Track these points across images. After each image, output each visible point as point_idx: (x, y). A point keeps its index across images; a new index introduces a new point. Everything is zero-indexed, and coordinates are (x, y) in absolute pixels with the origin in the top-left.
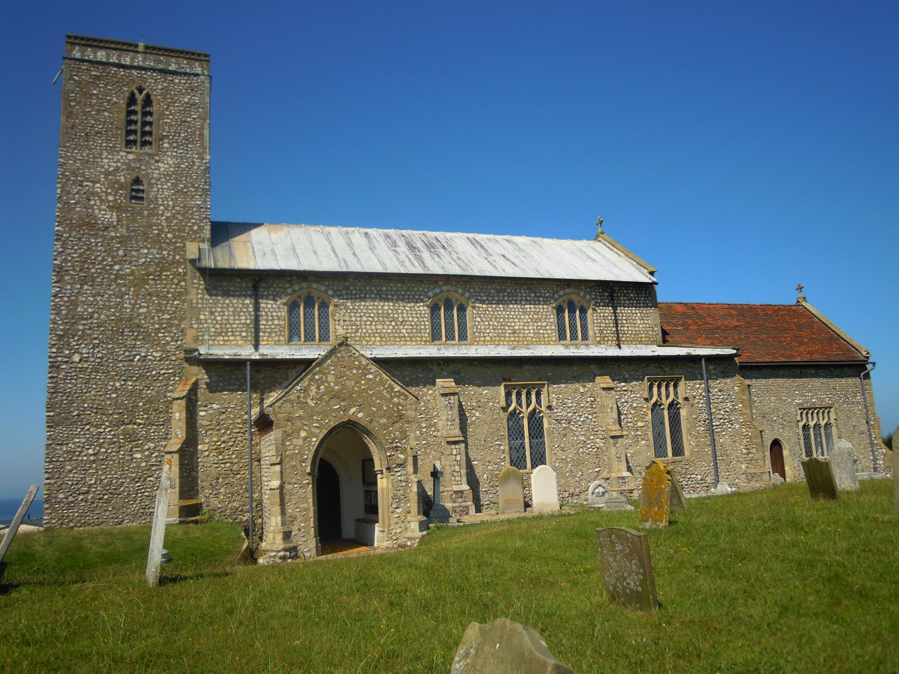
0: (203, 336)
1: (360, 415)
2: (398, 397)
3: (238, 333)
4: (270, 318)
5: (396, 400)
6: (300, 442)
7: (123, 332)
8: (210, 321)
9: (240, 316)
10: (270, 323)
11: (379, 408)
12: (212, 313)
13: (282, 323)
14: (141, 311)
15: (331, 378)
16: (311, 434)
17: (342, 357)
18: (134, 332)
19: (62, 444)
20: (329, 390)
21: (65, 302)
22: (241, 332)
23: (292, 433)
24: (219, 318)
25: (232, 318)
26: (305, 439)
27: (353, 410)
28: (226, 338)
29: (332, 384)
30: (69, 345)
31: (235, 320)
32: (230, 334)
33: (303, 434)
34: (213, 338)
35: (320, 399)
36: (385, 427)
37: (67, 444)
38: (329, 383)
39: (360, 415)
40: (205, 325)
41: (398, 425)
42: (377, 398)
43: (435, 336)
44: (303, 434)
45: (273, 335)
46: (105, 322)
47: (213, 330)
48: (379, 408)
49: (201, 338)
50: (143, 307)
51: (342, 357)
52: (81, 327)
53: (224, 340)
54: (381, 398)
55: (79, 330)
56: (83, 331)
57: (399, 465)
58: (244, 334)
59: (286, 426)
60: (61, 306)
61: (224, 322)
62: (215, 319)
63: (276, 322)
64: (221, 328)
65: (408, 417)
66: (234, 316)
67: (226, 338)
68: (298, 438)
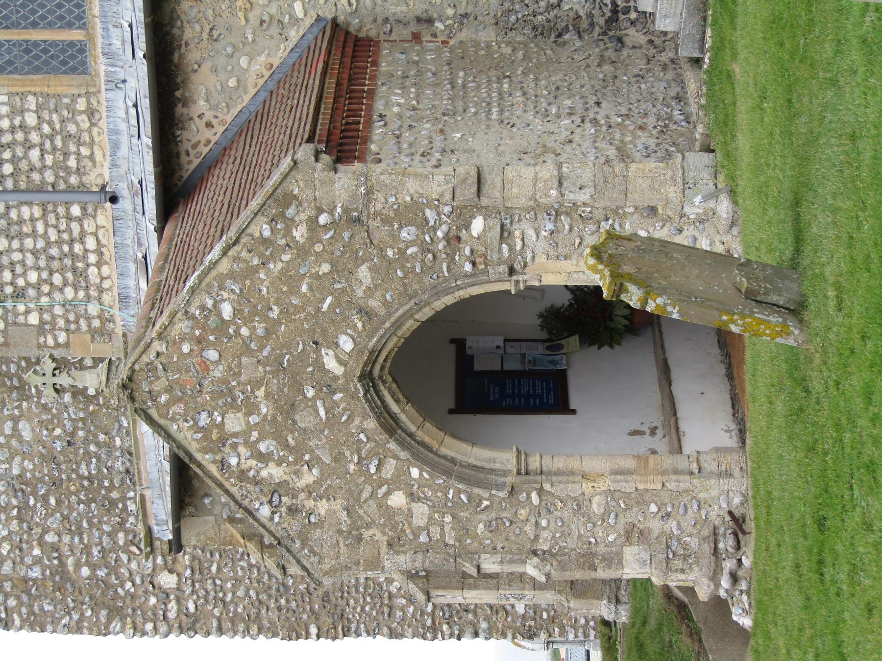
0: (88, 319)
1: (346, 343)
2: (291, 223)
3: (75, 226)
4: (20, 136)
5: (299, 233)
6: (421, 511)
7: (90, 478)
8: (44, 300)
9: (21, 222)
10: (35, 137)
11: (319, 283)
12: (19, 294)
13: (31, 102)
14: (27, 435)
15: (234, 422)
16: (400, 481)
17: (169, 390)
18: (87, 453)
19: (391, 608)
20: (276, 428)
21: (21, 604)
22: (69, 218)
23: (394, 528)
24: (33, 277)
25: (29, 243)
26: (412, 497)
27: (331, 363)
28: (92, 258)
29: (254, 419)
30: (133, 597)
31: (34, 234)
32: (78, 248)
33: (398, 499)
34: (93, 293)
35: (298, 451)
36: (384, 271)
37: (390, 596)
38: (250, 428)
39: (346, 343)
40: (58, 310)
41: (381, 233)
42: (294, 290)
43: (73, 60)
44: (398, 499)
45: (72, 128)
46: (65, 518)
47: (69, 292)
48: (319, 283)
49: (96, 323)
50: (15, 429)
51: (169, 390)
52: (85, 571)
53: (99, 265)
54: (289, 278)
55: (93, 576)
56: (93, 567)
57: (505, 234)
58: (76, 211)
59: (376, 544)
60: (31, 612)
61: (42, 263)
62: (37, 287)
63: (31, 119)
64: (62, 270)
65: (354, 196)
66: (21, 236)
67: (92, 258)
68: (410, 514)
